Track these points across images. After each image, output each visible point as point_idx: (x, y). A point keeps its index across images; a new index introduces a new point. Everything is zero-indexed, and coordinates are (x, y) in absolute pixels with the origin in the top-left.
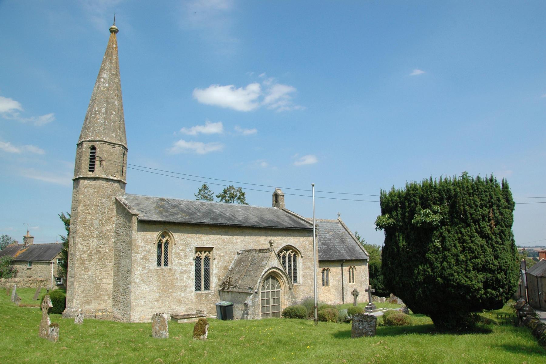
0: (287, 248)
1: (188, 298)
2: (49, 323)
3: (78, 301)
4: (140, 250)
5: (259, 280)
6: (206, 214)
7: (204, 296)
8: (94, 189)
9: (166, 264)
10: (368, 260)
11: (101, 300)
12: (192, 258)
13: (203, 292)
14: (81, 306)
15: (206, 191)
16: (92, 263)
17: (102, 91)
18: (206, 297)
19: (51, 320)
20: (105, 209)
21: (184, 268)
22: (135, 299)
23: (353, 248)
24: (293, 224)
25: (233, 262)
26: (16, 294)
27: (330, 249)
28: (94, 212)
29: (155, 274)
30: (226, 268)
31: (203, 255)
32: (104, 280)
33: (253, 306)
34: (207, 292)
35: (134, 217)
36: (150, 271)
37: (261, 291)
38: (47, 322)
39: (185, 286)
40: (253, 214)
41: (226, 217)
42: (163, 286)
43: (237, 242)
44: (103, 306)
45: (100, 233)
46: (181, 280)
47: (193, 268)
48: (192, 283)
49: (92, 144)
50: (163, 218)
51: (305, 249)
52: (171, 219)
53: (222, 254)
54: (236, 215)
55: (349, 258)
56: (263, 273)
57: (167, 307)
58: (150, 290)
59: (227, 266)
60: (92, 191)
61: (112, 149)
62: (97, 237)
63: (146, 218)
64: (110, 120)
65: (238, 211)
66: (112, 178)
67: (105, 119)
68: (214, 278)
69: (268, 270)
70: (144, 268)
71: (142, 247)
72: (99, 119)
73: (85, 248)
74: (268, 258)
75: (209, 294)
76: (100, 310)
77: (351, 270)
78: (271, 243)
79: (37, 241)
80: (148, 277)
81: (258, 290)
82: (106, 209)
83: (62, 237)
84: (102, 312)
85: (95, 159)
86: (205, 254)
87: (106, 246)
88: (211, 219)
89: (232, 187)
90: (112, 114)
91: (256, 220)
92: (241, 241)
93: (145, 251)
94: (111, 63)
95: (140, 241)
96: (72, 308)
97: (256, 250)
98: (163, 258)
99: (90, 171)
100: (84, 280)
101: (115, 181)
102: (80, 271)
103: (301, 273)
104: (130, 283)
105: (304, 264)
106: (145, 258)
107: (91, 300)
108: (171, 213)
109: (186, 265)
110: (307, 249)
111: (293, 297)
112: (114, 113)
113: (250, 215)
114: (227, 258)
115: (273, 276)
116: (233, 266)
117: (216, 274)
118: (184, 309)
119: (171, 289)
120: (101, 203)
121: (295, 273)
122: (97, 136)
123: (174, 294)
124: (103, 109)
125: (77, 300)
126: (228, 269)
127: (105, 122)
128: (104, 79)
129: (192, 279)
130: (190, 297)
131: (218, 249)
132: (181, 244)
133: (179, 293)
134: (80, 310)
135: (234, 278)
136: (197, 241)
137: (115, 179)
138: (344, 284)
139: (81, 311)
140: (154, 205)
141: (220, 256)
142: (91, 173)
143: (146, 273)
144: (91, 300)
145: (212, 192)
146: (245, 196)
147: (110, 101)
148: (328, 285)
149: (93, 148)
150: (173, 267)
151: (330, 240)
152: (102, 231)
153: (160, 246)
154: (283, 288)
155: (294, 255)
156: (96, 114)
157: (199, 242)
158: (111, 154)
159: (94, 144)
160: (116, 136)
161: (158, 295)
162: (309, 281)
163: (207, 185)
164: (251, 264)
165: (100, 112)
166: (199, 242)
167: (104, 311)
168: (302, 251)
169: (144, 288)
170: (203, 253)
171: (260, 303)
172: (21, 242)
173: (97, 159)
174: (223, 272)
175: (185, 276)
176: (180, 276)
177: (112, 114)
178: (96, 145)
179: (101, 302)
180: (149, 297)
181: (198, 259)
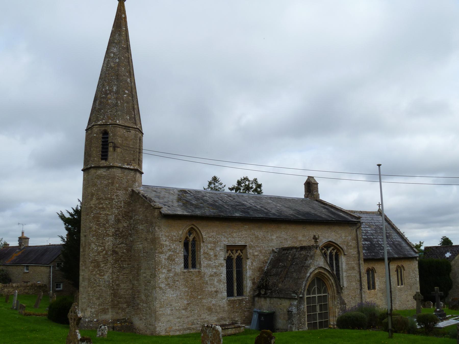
0: (329, 245)
1: (219, 306)
2: (79, 337)
3: (93, 310)
4: (165, 249)
5: (304, 283)
6: (234, 208)
7: (237, 303)
8: (108, 179)
9: (194, 266)
10: (418, 258)
11: (119, 309)
12: (222, 258)
13: (236, 299)
14: (97, 315)
15: (217, 184)
16: (109, 265)
17: (112, 68)
18: (240, 304)
19: (80, 333)
20: (121, 203)
21: (215, 270)
22: (161, 307)
23: (400, 245)
24: (333, 216)
25: (269, 262)
26: (17, 301)
27: (374, 245)
28: (109, 206)
29: (182, 277)
30: (260, 269)
31: (235, 256)
32: (122, 286)
33: (299, 314)
34: (240, 298)
35: (156, 210)
36: (176, 274)
37: (306, 296)
38: (76, 335)
39: (216, 292)
40: (286, 206)
41: (258, 210)
42: (191, 292)
43: (272, 239)
44: (121, 315)
45: (116, 231)
46: (211, 284)
47: (224, 270)
48: (223, 287)
49: (104, 129)
50: (189, 212)
51: (347, 245)
52: (198, 212)
53: (256, 254)
54: (268, 207)
55: (396, 256)
56: (308, 275)
57: (196, 317)
58: (177, 296)
59: (261, 267)
60: (106, 182)
61: (126, 134)
62: (113, 235)
63: (170, 212)
64: (123, 100)
65: (269, 203)
66: (127, 167)
67: (117, 99)
68: (248, 281)
69: (314, 271)
70: (169, 271)
71: (167, 246)
72: (110, 99)
73: (100, 249)
74: (312, 257)
75: (242, 300)
76: (118, 320)
77: (399, 271)
78: (315, 238)
79: (32, 243)
80: (174, 281)
81: (303, 295)
82: (123, 203)
83: (62, 238)
84: (121, 323)
85: (107, 145)
86: (237, 254)
87: (123, 245)
88: (242, 211)
89: (246, 179)
90: (125, 93)
91: (291, 212)
92: (277, 237)
93: (169, 250)
94: (120, 35)
95: (164, 239)
96: (86, 318)
97: (296, 248)
98: (191, 260)
99: (102, 159)
100: (99, 286)
101: (132, 170)
102: (95, 275)
103: (345, 274)
104: (154, 288)
105: (347, 264)
106: (171, 259)
107: (108, 309)
108: (197, 207)
109: (216, 267)
110: (351, 246)
111: (343, 303)
112: (126, 92)
113: (283, 208)
114: (262, 257)
115: (319, 280)
116: (269, 267)
117: (250, 277)
118: (215, 318)
119: (200, 295)
120: (117, 196)
121: (338, 274)
122: (109, 118)
123: (204, 301)
124: (115, 88)
125: (92, 308)
126: (263, 270)
127: (117, 103)
128: (114, 54)
129: (224, 283)
130: (222, 304)
131: (251, 247)
132: (210, 243)
133: (210, 299)
134: (95, 320)
135: (272, 280)
136: (228, 238)
137: (132, 167)
138: (392, 287)
139: (97, 321)
140: (176, 197)
141: (254, 255)
142: (103, 161)
143: (172, 277)
144: (108, 309)
145: (223, 185)
146: (262, 188)
147: (121, 78)
148: (374, 288)
149: (105, 133)
150: (202, 269)
151: (373, 235)
152: (119, 229)
153: (186, 245)
154: (330, 292)
155: (336, 253)
156: (106, 94)
157: (230, 239)
158: (126, 139)
159: (106, 128)
160: (130, 118)
161: (186, 302)
162: (354, 284)
163: (218, 176)
164: (291, 265)
165: (111, 91)
166: (230, 239)
167: (123, 321)
168: (345, 248)
169: (171, 294)
170: (234, 252)
171: (306, 310)
172: (16, 244)
173: (111, 145)
174: (257, 274)
175: (216, 280)
176: (210, 280)
177: (125, 93)
178: (109, 129)
179: (120, 311)
180: (176, 305)
181: (229, 260)
